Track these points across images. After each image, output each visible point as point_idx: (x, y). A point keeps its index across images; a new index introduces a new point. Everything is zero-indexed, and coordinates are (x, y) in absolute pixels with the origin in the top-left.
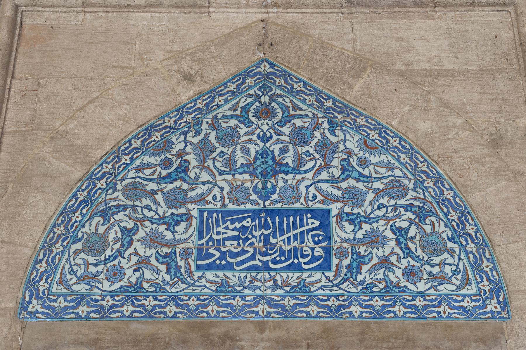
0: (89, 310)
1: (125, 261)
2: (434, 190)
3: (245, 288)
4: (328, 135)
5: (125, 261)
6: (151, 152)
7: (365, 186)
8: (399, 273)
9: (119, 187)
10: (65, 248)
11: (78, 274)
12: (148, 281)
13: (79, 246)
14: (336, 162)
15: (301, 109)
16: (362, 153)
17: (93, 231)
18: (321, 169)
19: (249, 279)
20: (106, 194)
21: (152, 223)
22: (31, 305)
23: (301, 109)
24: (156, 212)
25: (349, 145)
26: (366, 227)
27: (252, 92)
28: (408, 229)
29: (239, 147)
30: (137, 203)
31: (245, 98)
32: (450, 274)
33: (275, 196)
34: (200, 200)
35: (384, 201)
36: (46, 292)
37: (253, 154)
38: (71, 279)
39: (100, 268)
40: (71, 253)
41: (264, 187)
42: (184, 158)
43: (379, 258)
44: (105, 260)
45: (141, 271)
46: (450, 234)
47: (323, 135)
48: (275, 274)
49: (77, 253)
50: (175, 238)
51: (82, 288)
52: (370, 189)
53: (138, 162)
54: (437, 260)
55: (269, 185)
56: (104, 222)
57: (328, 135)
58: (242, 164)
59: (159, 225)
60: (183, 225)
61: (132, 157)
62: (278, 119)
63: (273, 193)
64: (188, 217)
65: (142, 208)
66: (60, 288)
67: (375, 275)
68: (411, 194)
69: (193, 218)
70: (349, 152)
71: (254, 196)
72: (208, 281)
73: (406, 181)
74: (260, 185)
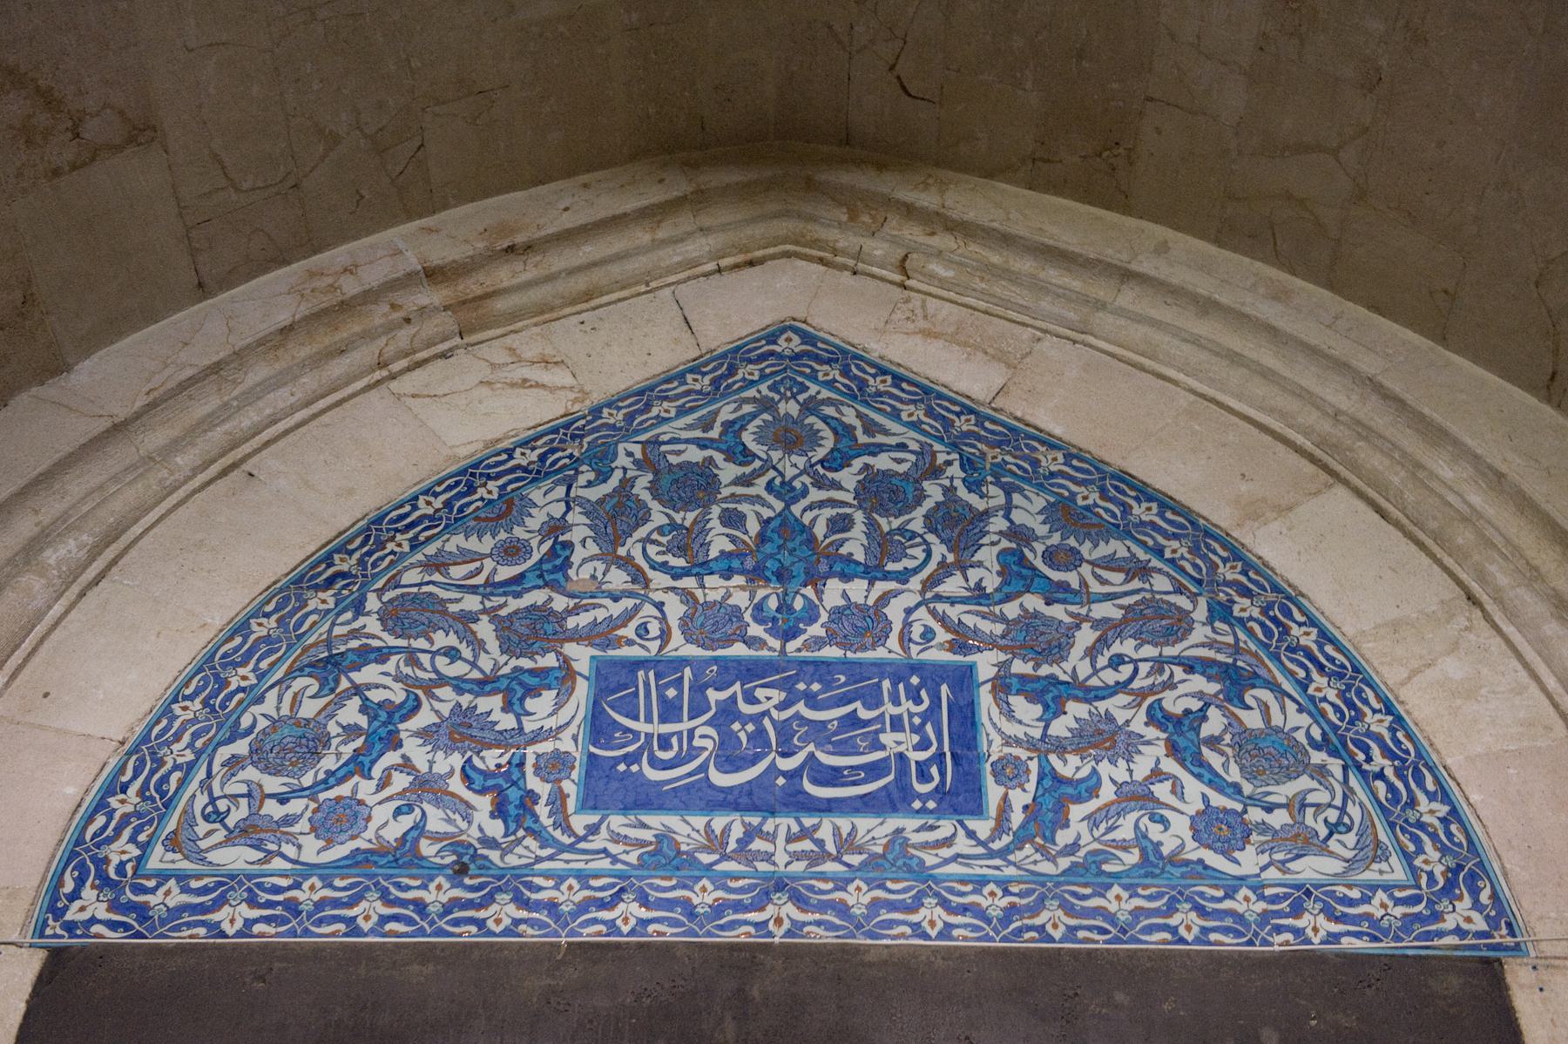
0: (256, 913)
1: (371, 785)
2: (1262, 625)
3: (725, 857)
4: (962, 492)
5: (371, 785)
6: (473, 523)
7: (1071, 614)
8: (1181, 826)
9: (373, 603)
10: (198, 754)
11: (231, 821)
12: (436, 837)
13: (241, 747)
14: (987, 555)
15: (886, 432)
16: (1056, 539)
17: (285, 711)
18: (945, 570)
19: (737, 832)
20: (333, 624)
21: (460, 691)
22: (77, 904)
23: (886, 432)
24: (474, 665)
25: (1018, 517)
26: (1077, 710)
27: (751, 393)
28: (1202, 716)
29: (716, 511)
30: (421, 643)
31: (734, 405)
32: (1323, 832)
33: (816, 630)
34: (602, 635)
35: (1127, 647)
36: (129, 867)
37: (753, 527)
38: (209, 834)
39: (296, 806)
40: (216, 768)
41: (785, 607)
42: (561, 538)
43: (1119, 786)
44: (316, 784)
45: (417, 811)
46: (1316, 733)
47: (949, 491)
48: (815, 821)
49: (234, 763)
50: (521, 729)
51: (238, 857)
52: (1087, 618)
53: (431, 549)
54: (1283, 792)
55: (798, 604)
56: (320, 690)
57: (962, 492)
58: (722, 552)
59: (477, 695)
60: (549, 696)
61: (416, 537)
62: (821, 453)
63: (813, 619)
64: (566, 675)
65: (434, 654)
66: (170, 856)
67: (1110, 829)
68: (1200, 633)
69: (579, 679)
70: (1020, 535)
71: (755, 630)
72: (616, 838)
73: (1183, 602)
74: (773, 603)
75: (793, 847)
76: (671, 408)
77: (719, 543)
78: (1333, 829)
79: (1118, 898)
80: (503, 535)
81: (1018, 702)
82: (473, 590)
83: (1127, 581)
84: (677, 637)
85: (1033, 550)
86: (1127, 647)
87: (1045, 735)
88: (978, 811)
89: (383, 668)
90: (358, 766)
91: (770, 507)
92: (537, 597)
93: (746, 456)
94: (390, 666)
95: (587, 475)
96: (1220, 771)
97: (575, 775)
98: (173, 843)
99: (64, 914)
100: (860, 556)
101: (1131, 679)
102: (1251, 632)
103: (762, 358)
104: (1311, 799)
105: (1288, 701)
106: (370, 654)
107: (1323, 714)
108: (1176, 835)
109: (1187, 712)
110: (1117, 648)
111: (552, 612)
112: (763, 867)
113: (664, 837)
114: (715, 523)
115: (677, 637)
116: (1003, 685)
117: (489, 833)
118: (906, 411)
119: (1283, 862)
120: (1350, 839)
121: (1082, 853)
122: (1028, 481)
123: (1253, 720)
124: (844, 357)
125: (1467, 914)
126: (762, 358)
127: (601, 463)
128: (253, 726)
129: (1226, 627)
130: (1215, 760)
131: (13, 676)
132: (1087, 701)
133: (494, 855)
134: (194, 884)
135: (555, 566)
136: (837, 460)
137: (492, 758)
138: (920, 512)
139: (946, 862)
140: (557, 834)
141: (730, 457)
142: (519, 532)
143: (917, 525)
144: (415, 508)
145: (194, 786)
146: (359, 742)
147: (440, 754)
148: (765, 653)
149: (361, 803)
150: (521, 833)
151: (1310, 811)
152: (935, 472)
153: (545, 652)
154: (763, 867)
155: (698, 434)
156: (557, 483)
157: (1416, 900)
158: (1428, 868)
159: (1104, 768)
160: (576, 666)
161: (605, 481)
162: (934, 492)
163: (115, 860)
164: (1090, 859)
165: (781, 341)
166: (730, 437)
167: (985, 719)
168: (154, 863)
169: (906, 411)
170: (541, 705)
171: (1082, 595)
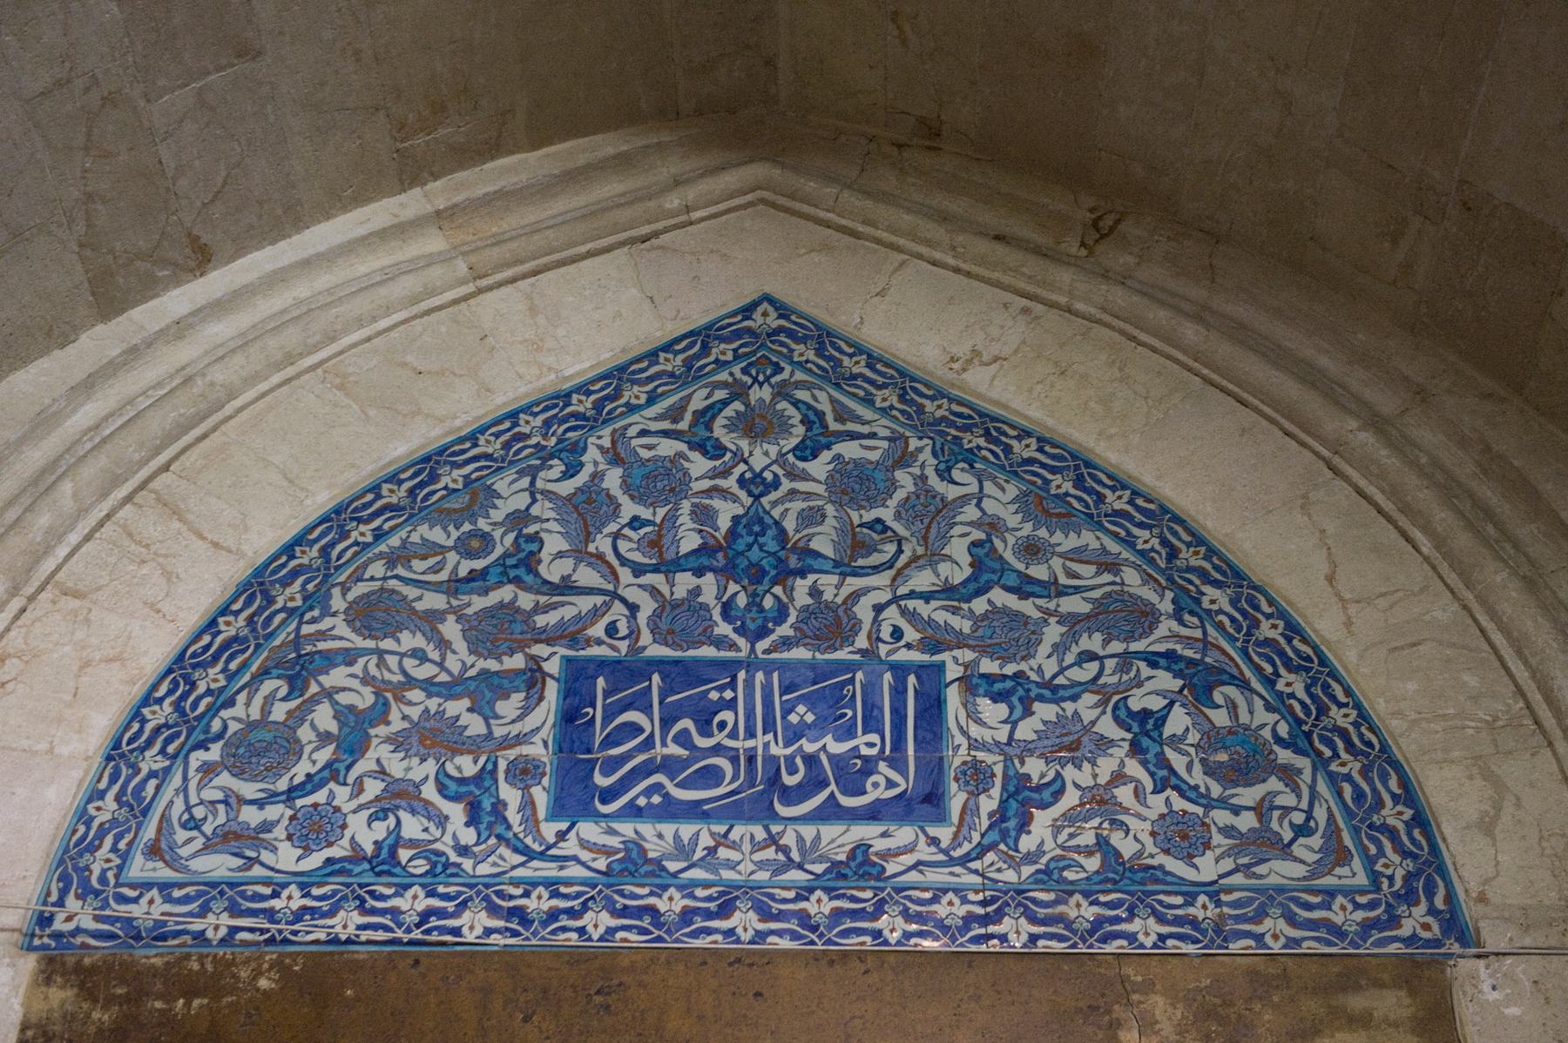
4: (934, 481)
7: (1039, 608)
9: (338, 603)
11: (208, 828)
12: (412, 843)
13: (214, 753)
14: (958, 549)
19: (706, 841)
24: (441, 665)
27: (723, 376)
29: (686, 506)
30: (387, 644)
32: (1287, 835)
33: (785, 630)
34: (571, 634)
35: (1093, 642)
36: (110, 875)
40: (191, 773)
41: (755, 602)
44: (291, 790)
46: (1283, 729)
49: (208, 770)
50: (490, 733)
53: (394, 541)
54: (1248, 795)
55: (768, 602)
56: (289, 694)
57: (934, 481)
60: (517, 698)
62: (794, 441)
64: (533, 678)
65: (402, 655)
66: (150, 865)
67: (1072, 836)
68: (1167, 626)
69: (548, 680)
70: (993, 526)
71: (724, 629)
72: (584, 844)
74: (742, 600)
75: (758, 856)
78: (1302, 831)
79: (1343, 908)
80: (467, 527)
81: (984, 704)
82: (436, 587)
83: (1098, 574)
84: (646, 638)
85: (1005, 541)
86: (1093, 642)
88: (941, 818)
89: (350, 670)
90: (332, 772)
92: (506, 593)
94: (357, 669)
95: (558, 468)
96: (1185, 775)
97: (545, 781)
98: (154, 851)
100: (828, 551)
102: (1220, 626)
103: (737, 334)
104: (1279, 801)
105: (1256, 698)
106: (329, 660)
107: (1291, 709)
111: (518, 610)
112: (727, 875)
113: (635, 848)
114: (685, 519)
115: (646, 638)
116: (971, 683)
118: (879, 395)
120: (1316, 841)
121: (1044, 860)
123: (1220, 718)
124: (823, 337)
125: (1422, 920)
126: (737, 334)
128: (225, 727)
129: (1195, 620)
130: (1178, 761)
131: (16, 618)
132: (1057, 702)
133: (467, 864)
135: (522, 563)
136: (806, 451)
137: (467, 766)
140: (529, 841)
141: (700, 447)
143: (886, 514)
145: (168, 793)
149: (337, 810)
150: (493, 841)
152: (904, 459)
153: (512, 653)
155: (666, 425)
156: (521, 473)
157: (1372, 905)
158: (1389, 872)
159: (1069, 772)
160: (546, 666)
163: (96, 870)
164: (1052, 865)
165: (757, 315)
167: (952, 724)
169: (879, 395)
170: (508, 707)
171: (1054, 589)
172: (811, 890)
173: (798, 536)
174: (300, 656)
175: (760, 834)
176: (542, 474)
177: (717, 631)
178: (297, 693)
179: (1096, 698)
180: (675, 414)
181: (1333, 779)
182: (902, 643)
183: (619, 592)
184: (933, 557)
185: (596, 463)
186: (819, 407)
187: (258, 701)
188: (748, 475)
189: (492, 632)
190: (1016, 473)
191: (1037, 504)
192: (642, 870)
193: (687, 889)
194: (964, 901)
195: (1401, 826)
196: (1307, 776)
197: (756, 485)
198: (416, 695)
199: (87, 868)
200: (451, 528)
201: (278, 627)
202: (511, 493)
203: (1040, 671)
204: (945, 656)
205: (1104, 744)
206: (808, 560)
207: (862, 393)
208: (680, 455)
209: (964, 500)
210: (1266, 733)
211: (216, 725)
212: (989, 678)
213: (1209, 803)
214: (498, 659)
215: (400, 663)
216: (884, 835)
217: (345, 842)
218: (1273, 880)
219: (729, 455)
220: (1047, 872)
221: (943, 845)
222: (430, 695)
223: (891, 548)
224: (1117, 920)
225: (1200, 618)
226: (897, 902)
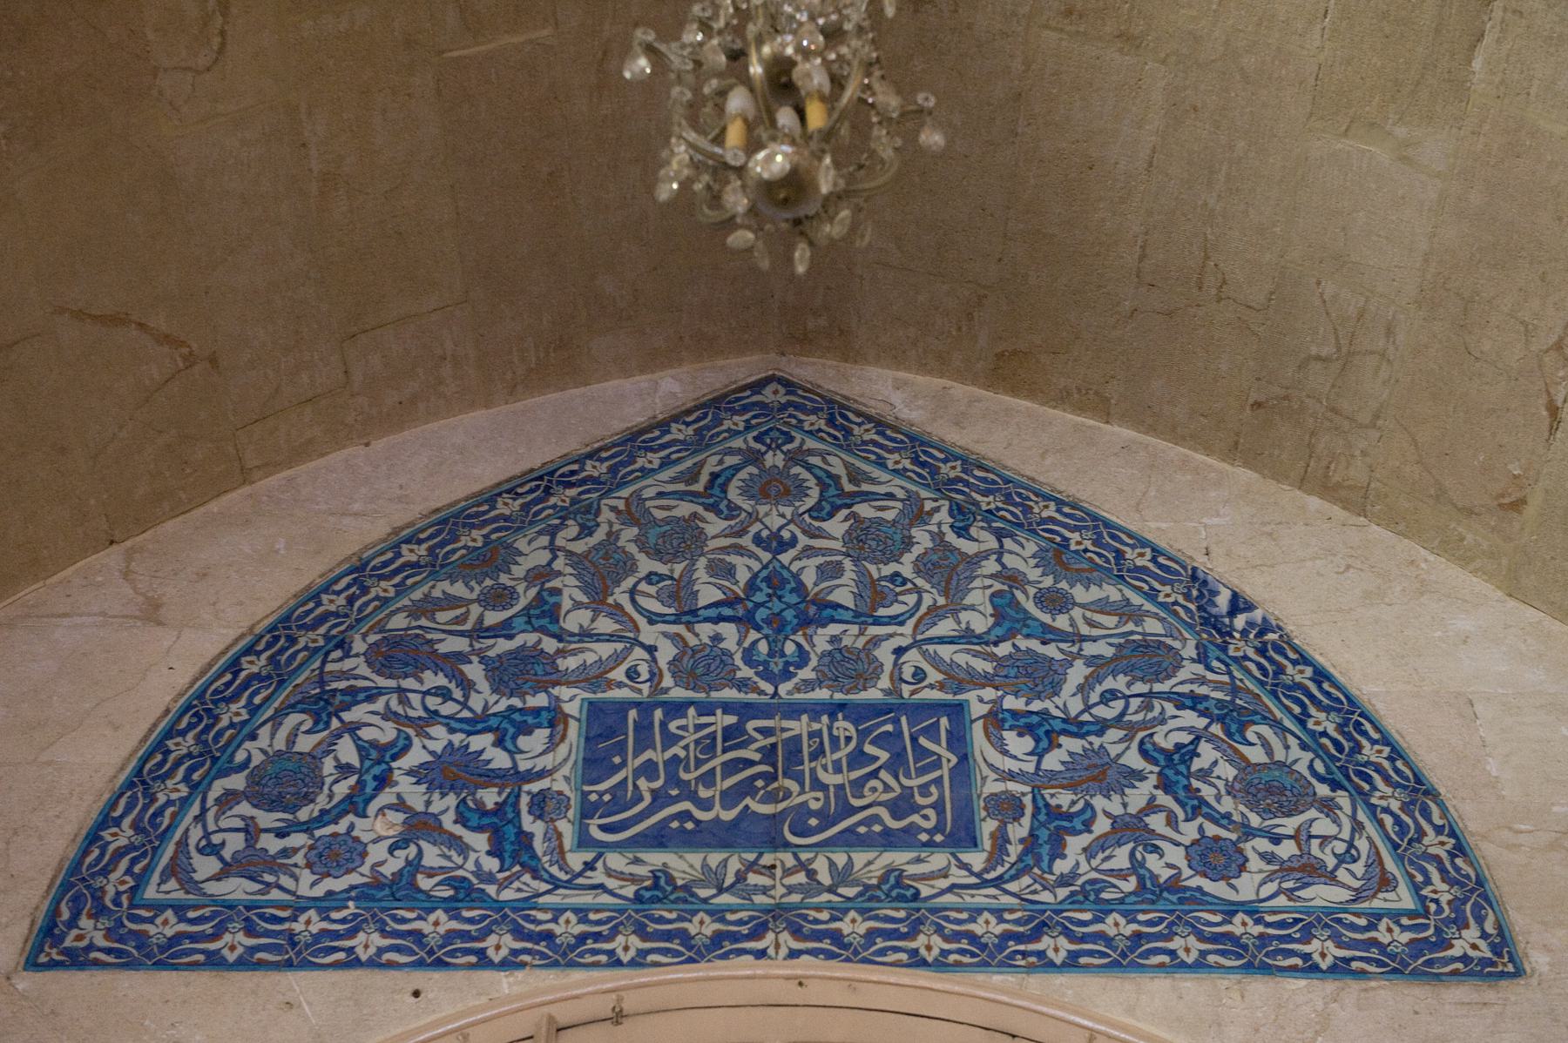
4: (951, 537)
9: (359, 646)
13: (237, 782)
15: (873, 481)
16: (1048, 582)
19: (734, 865)
20: (324, 663)
21: (452, 731)
23: (873, 481)
24: (465, 705)
26: (1071, 744)
27: (738, 443)
30: (409, 683)
32: (1331, 862)
33: (806, 673)
34: (594, 678)
35: (1119, 683)
36: (124, 899)
40: (210, 802)
42: (548, 585)
47: (938, 537)
48: (811, 855)
51: (237, 889)
53: (417, 595)
54: (1289, 825)
55: (790, 648)
57: (951, 537)
59: (469, 734)
60: (542, 734)
62: (810, 502)
64: (555, 718)
65: (425, 693)
68: (1190, 670)
70: (1013, 579)
71: (745, 672)
72: (609, 873)
74: (763, 647)
75: (787, 881)
76: (655, 459)
77: (708, 594)
78: (1348, 857)
80: (488, 582)
81: (1010, 737)
84: (668, 681)
85: (1025, 592)
86: (1119, 683)
87: (1038, 767)
89: (372, 707)
90: (355, 804)
91: (758, 559)
93: (734, 509)
94: (379, 705)
95: (572, 530)
97: (571, 814)
98: (171, 871)
99: (62, 941)
100: (848, 601)
101: (1123, 714)
105: (1289, 737)
106: (354, 696)
107: (1322, 746)
108: (1167, 862)
109: (1179, 747)
110: (1109, 683)
112: (759, 899)
114: (701, 573)
115: (668, 681)
117: (486, 868)
118: (891, 459)
119: (1292, 890)
120: (1358, 869)
122: (1020, 525)
123: (1256, 755)
127: (587, 518)
128: (249, 759)
134: (191, 914)
135: (545, 613)
137: (490, 797)
138: (908, 558)
139: (942, 892)
140: (554, 870)
141: (713, 508)
142: (504, 579)
143: (906, 570)
144: (399, 555)
145: (188, 819)
146: (353, 780)
147: (436, 796)
148: (753, 697)
149: (357, 840)
150: (518, 868)
151: (1315, 843)
152: (919, 516)
154: (759, 899)
155: (681, 487)
156: (540, 533)
159: (1099, 802)
161: (590, 534)
162: (922, 539)
166: (716, 491)
167: (977, 754)
168: (150, 893)
169: (891, 459)
172: (846, 911)
173: (817, 589)
174: (324, 692)
175: (789, 861)
176: (561, 534)
177: (739, 675)
178: (321, 726)
179: (1122, 733)
180: (692, 476)
181: (1372, 809)
182: (925, 683)
183: (641, 639)
184: (954, 610)
185: (611, 524)
186: (834, 471)
187: (282, 734)
188: (765, 533)
189: (514, 672)
190: (1034, 532)
191: (1057, 557)
192: (672, 897)
193: (718, 914)
194: (1001, 920)
195: (1444, 855)
196: (1348, 809)
197: (777, 544)
198: (438, 731)
199: (102, 889)
200: (473, 583)
201: (301, 665)
202: (532, 552)
203: (1065, 709)
204: (971, 696)
205: (1140, 776)
206: (825, 611)
207: (873, 457)
208: (695, 515)
209: (984, 555)
210: (1302, 767)
211: (240, 756)
212: (1015, 714)
213: (1249, 833)
214: (522, 696)
215: (423, 703)
216: (919, 860)
217: (365, 869)
218: (1318, 903)
219: (744, 515)
220: (1083, 891)
221: (976, 869)
222: (452, 731)
223: (911, 599)
224: (1288, 939)
225: (1227, 665)
226: (1326, 925)
